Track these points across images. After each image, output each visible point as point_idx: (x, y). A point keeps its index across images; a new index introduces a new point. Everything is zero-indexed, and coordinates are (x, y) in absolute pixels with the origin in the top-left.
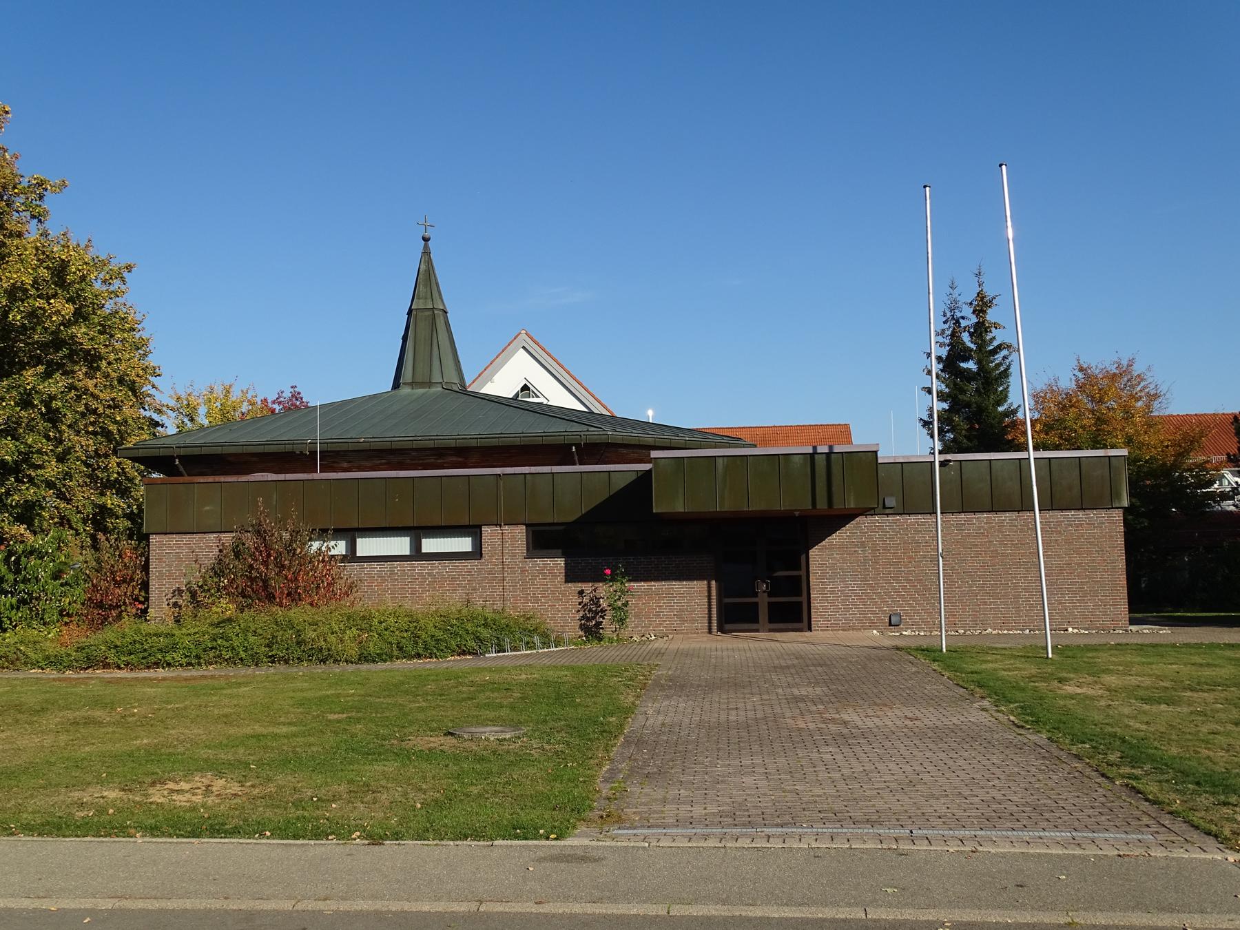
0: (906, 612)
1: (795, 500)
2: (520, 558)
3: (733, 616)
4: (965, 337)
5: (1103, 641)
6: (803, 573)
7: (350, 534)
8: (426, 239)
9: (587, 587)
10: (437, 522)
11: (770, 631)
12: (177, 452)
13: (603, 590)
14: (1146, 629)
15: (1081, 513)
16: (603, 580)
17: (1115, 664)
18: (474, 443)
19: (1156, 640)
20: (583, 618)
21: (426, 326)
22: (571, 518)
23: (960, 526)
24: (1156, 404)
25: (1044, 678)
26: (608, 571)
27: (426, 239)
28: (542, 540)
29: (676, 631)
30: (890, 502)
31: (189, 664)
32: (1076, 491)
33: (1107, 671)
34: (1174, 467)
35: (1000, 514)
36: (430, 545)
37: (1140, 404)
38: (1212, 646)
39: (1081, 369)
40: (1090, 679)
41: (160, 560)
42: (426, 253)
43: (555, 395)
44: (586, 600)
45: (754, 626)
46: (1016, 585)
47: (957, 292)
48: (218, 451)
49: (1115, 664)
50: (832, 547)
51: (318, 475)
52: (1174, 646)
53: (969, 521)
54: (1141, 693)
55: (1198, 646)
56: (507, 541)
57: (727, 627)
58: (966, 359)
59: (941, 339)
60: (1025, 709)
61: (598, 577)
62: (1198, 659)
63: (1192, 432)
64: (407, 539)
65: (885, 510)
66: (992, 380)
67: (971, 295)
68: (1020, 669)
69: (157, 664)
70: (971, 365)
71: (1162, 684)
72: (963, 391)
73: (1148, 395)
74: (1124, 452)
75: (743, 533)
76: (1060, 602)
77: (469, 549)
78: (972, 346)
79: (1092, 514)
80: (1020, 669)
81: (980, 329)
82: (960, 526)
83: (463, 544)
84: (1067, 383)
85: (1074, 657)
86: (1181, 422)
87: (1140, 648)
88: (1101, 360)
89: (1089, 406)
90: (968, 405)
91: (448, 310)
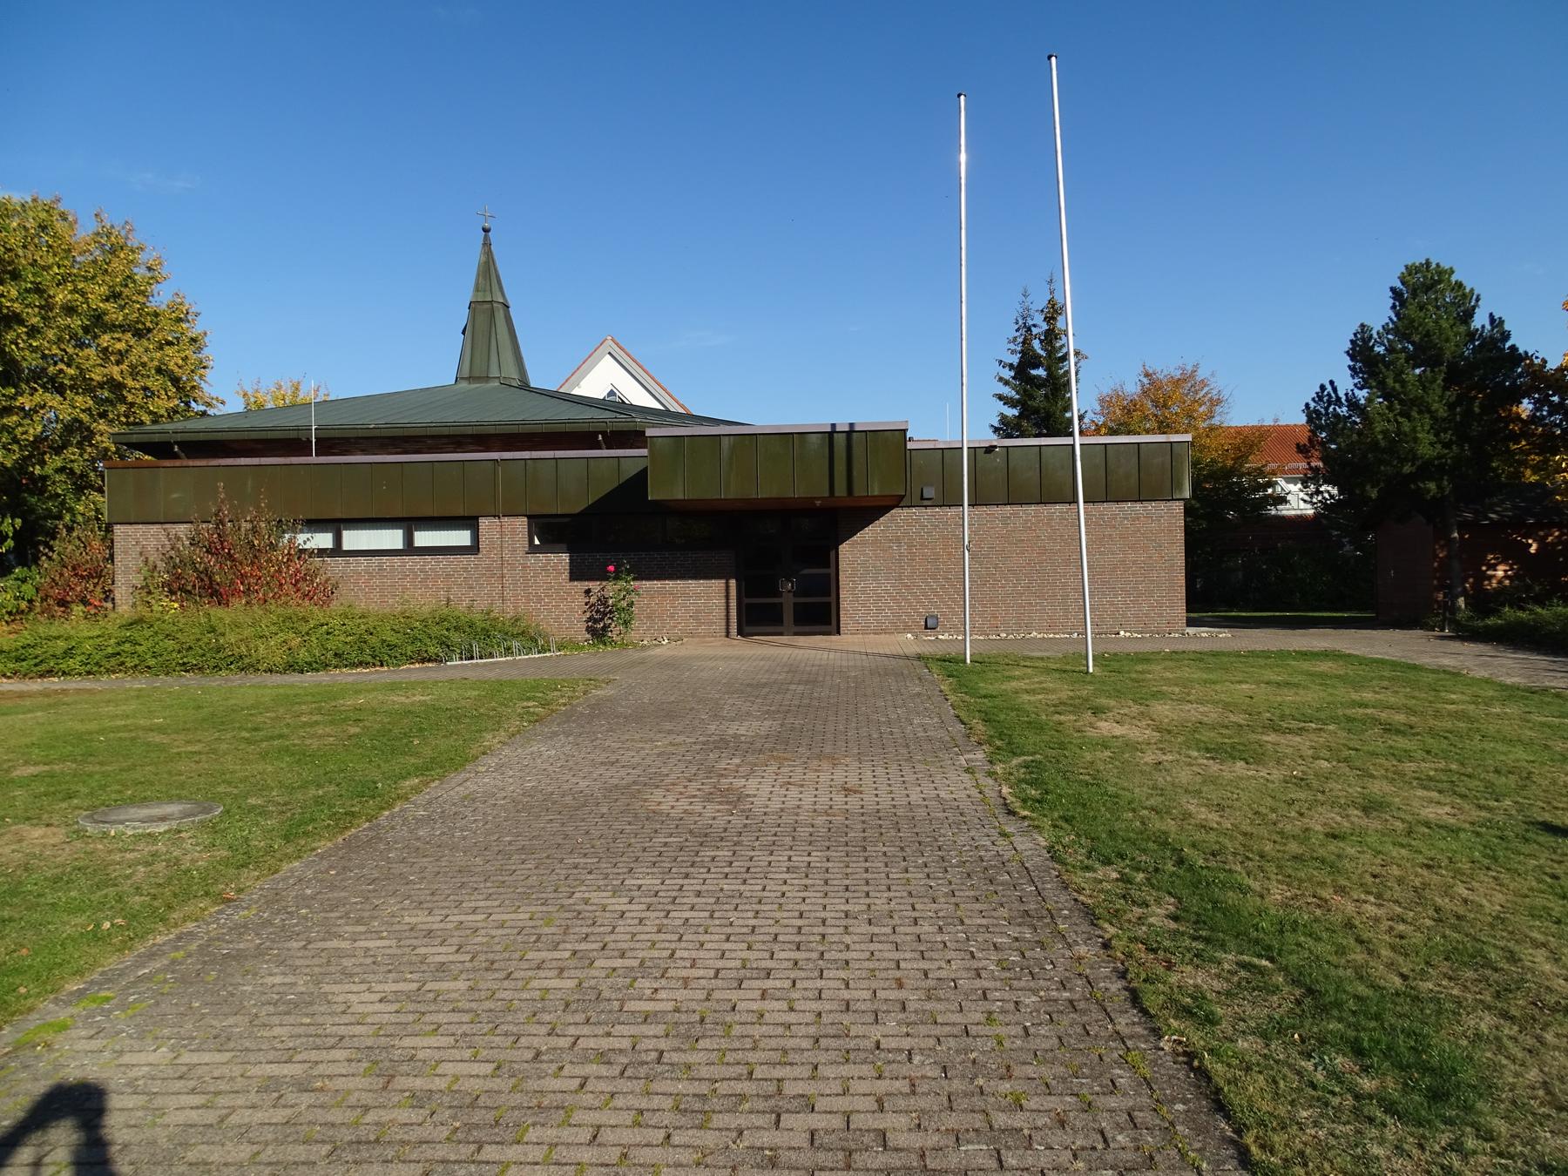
0: (944, 614)
1: (808, 485)
2: (520, 553)
3: (755, 618)
4: (1036, 344)
5: (1156, 647)
6: (832, 571)
7: (335, 525)
8: (486, 230)
9: (595, 586)
10: (429, 513)
11: (796, 634)
12: (179, 437)
13: (611, 589)
14: (1204, 632)
15: (1138, 506)
16: (607, 579)
17: (1168, 681)
18: (492, 430)
19: (1216, 647)
20: (590, 619)
21: (488, 320)
22: (577, 510)
23: (1005, 520)
24: (1218, 409)
25: (1076, 706)
26: (611, 568)
27: (486, 230)
28: (551, 531)
29: (692, 635)
30: (929, 492)
31: (89, 673)
32: (1134, 480)
33: (1158, 695)
34: (1231, 472)
35: (1049, 507)
36: (423, 538)
37: (1202, 409)
38: (1283, 655)
39: (1147, 375)
40: (1136, 709)
41: (126, 553)
42: (487, 244)
43: (638, 397)
44: (593, 600)
45: (779, 629)
46: (1065, 585)
47: (1029, 299)
48: (219, 436)
49: (1168, 681)
50: (864, 543)
51: (314, 459)
52: (1238, 655)
53: (1015, 514)
54: (1206, 736)
55: (1266, 655)
56: (507, 534)
57: (747, 629)
58: (1036, 367)
59: (1012, 346)
60: (1034, 774)
61: (603, 577)
62: (1270, 675)
63: (1251, 440)
64: (400, 532)
65: (923, 502)
66: (1058, 387)
67: (1042, 303)
68: (1046, 691)
69: (50, 673)
70: (1041, 372)
71: (1233, 718)
72: (1032, 397)
73: (1211, 400)
74: (1188, 437)
75: (773, 531)
76: (1112, 604)
77: (468, 543)
78: (1043, 353)
79: (1150, 506)
80: (1046, 691)
81: (1051, 336)
82: (1005, 520)
83: (462, 538)
84: (1132, 388)
85: (1125, 673)
86: (1239, 431)
87: (1199, 657)
88: (1167, 366)
89: (1153, 410)
90: (1036, 411)
91: (510, 303)
